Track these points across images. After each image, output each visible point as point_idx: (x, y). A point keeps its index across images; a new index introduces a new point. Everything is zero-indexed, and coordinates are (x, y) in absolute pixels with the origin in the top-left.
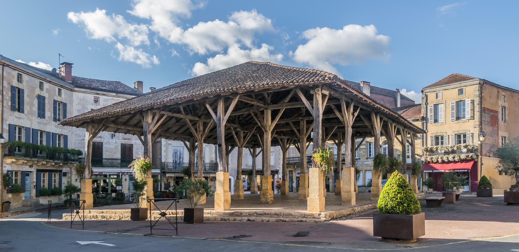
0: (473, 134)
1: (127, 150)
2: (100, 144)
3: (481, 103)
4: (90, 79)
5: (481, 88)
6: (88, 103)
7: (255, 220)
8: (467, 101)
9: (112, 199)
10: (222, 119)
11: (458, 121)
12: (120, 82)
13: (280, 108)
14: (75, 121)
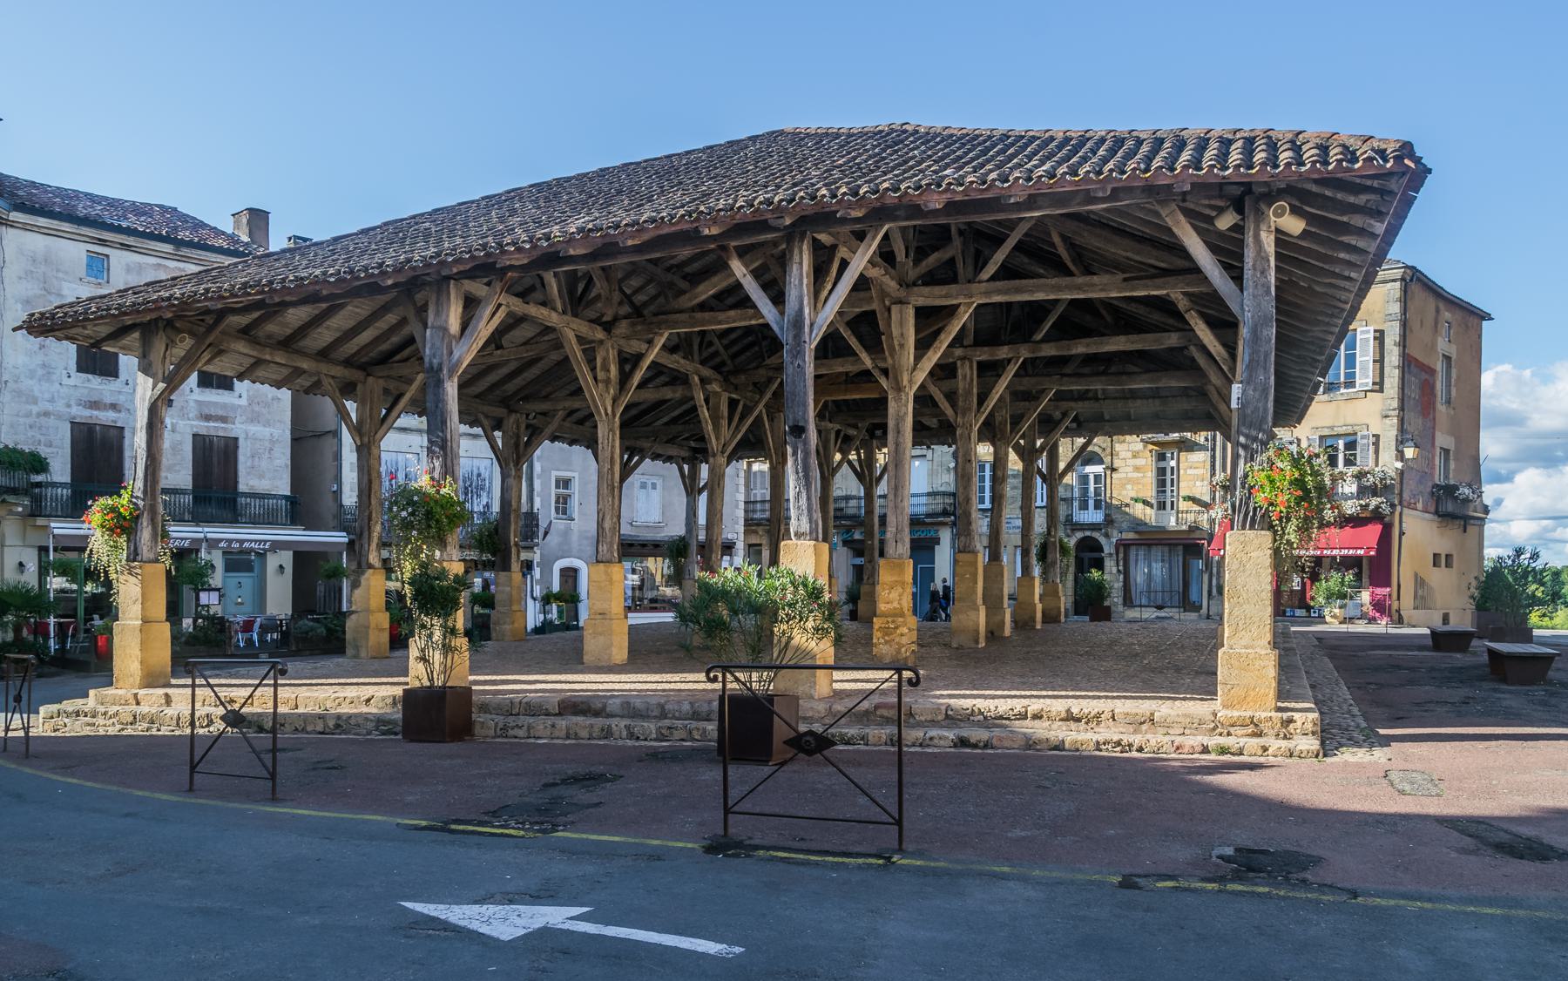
0: (1377, 437)
1: (215, 459)
2: (113, 433)
3: (1403, 343)
4: (58, 188)
5: (1405, 292)
6: (66, 273)
7: (995, 742)
8: (1363, 332)
9: (183, 639)
10: (807, 322)
11: (1332, 395)
12: (175, 209)
13: (955, 302)
14: (102, 317)
